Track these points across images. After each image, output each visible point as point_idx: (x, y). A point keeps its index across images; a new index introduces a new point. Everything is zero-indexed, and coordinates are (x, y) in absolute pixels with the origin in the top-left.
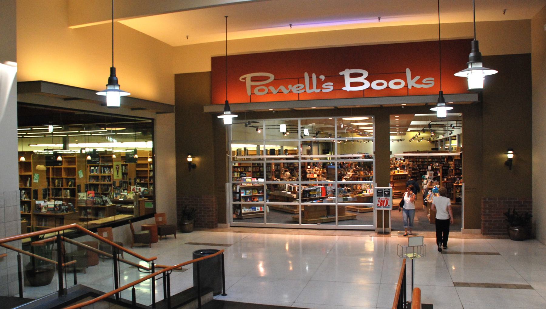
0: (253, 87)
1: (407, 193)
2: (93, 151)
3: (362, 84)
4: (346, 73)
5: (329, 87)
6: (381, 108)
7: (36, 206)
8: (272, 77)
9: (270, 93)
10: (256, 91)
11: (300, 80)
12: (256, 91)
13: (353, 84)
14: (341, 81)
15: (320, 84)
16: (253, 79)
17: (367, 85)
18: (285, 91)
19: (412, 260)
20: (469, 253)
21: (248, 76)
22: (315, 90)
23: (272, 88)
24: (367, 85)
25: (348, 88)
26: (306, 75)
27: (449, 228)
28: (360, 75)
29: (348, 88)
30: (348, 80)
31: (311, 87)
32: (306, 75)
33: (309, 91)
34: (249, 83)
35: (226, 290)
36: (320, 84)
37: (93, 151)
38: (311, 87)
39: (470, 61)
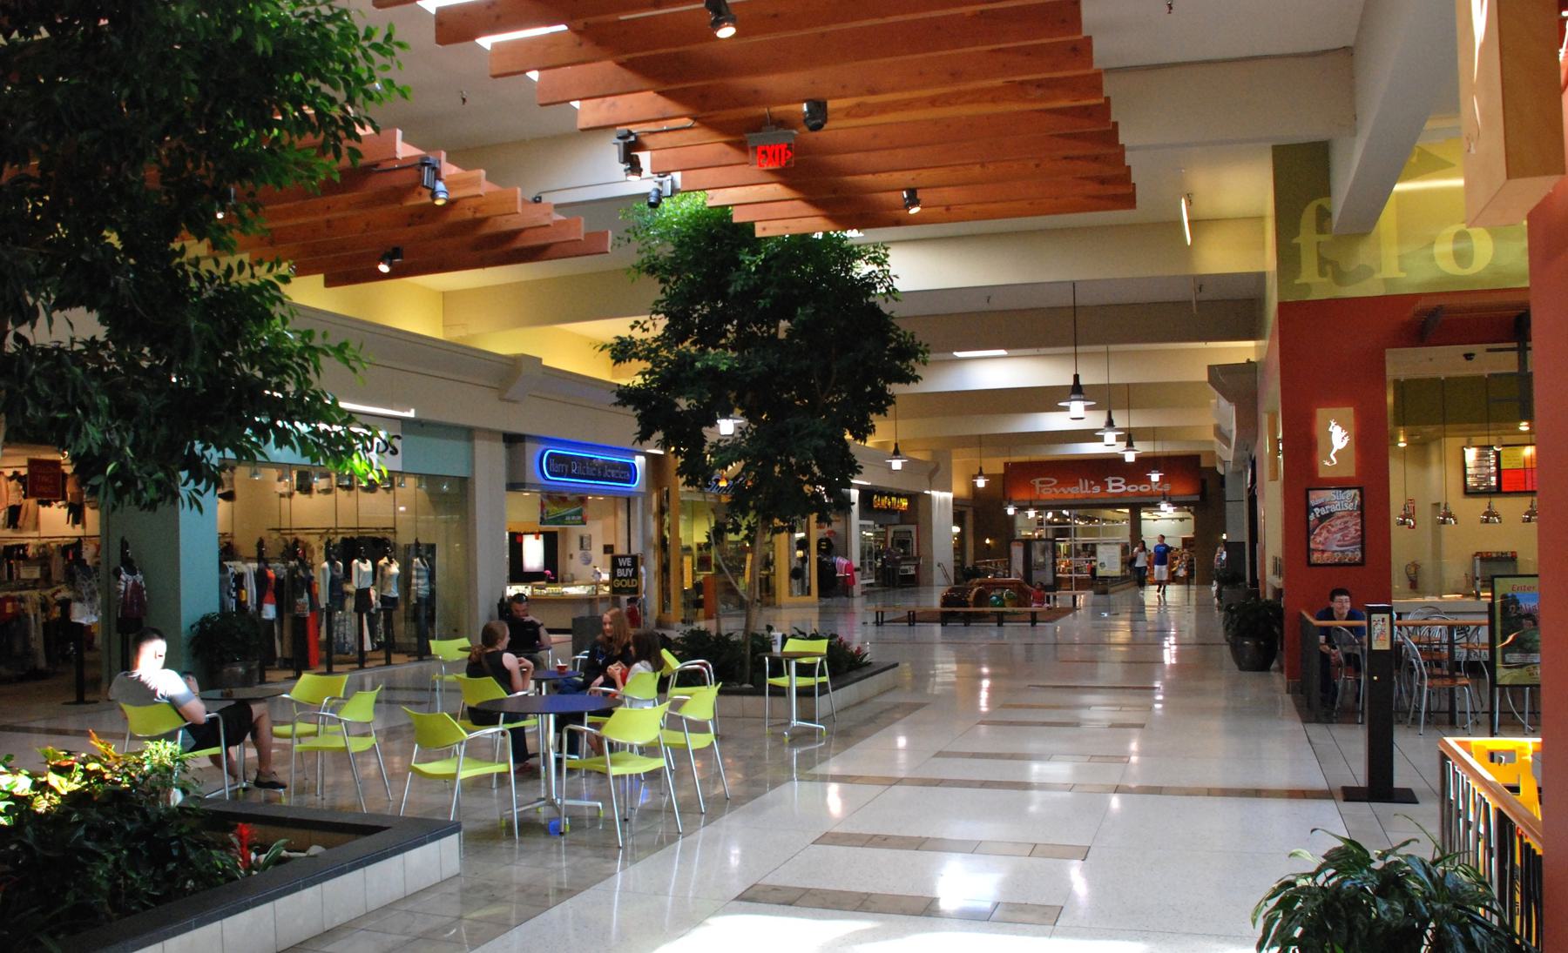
0: (1040, 488)
1: (815, 515)
2: (94, 311)
3: (1120, 488)
4: (1109, 480)
5: (1097, 489)
6: (1136, 504)
7: (1535, 712)
8: (1055, 481)
9: (1054, 492)
10: (1043, 491)
11: (1077, 484)
12: (1043, 491)
13: (1114, 488)
14: (1105, 486)
15: (1090, 487)
16: (1040, 483)
17: (1124, 488)
18: (1066, 492)
19: (427, 690)
20: (1180, 794)
21: (1037, 480)
22: (1088, 491)
23: (1055, 490)
24: (1124, 488)
25: (1110, 490)
26: (1081, 481)
27: (1543, 755)
28: (1119, 481)
29: (1110, 490)
30: (1111, 485)
31: (1084, 489)
32: (1081, 481)
33: (1082, 492)
34: (1038, 486)
35: (1373, 804)
36: (1090, 487)
37: (94, 311)
38: (1084, 489)
39: (1481, 568)
